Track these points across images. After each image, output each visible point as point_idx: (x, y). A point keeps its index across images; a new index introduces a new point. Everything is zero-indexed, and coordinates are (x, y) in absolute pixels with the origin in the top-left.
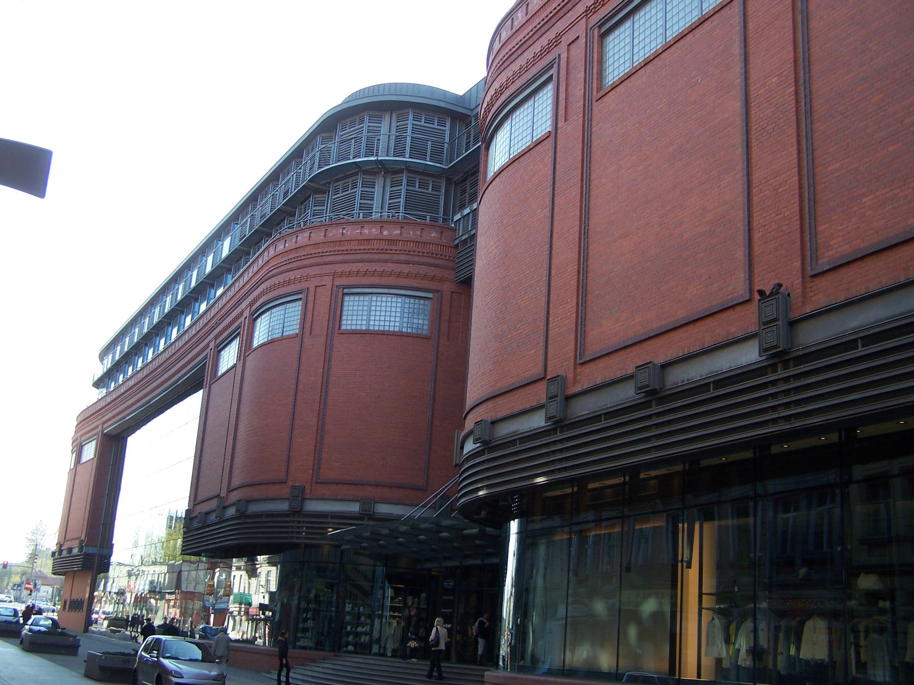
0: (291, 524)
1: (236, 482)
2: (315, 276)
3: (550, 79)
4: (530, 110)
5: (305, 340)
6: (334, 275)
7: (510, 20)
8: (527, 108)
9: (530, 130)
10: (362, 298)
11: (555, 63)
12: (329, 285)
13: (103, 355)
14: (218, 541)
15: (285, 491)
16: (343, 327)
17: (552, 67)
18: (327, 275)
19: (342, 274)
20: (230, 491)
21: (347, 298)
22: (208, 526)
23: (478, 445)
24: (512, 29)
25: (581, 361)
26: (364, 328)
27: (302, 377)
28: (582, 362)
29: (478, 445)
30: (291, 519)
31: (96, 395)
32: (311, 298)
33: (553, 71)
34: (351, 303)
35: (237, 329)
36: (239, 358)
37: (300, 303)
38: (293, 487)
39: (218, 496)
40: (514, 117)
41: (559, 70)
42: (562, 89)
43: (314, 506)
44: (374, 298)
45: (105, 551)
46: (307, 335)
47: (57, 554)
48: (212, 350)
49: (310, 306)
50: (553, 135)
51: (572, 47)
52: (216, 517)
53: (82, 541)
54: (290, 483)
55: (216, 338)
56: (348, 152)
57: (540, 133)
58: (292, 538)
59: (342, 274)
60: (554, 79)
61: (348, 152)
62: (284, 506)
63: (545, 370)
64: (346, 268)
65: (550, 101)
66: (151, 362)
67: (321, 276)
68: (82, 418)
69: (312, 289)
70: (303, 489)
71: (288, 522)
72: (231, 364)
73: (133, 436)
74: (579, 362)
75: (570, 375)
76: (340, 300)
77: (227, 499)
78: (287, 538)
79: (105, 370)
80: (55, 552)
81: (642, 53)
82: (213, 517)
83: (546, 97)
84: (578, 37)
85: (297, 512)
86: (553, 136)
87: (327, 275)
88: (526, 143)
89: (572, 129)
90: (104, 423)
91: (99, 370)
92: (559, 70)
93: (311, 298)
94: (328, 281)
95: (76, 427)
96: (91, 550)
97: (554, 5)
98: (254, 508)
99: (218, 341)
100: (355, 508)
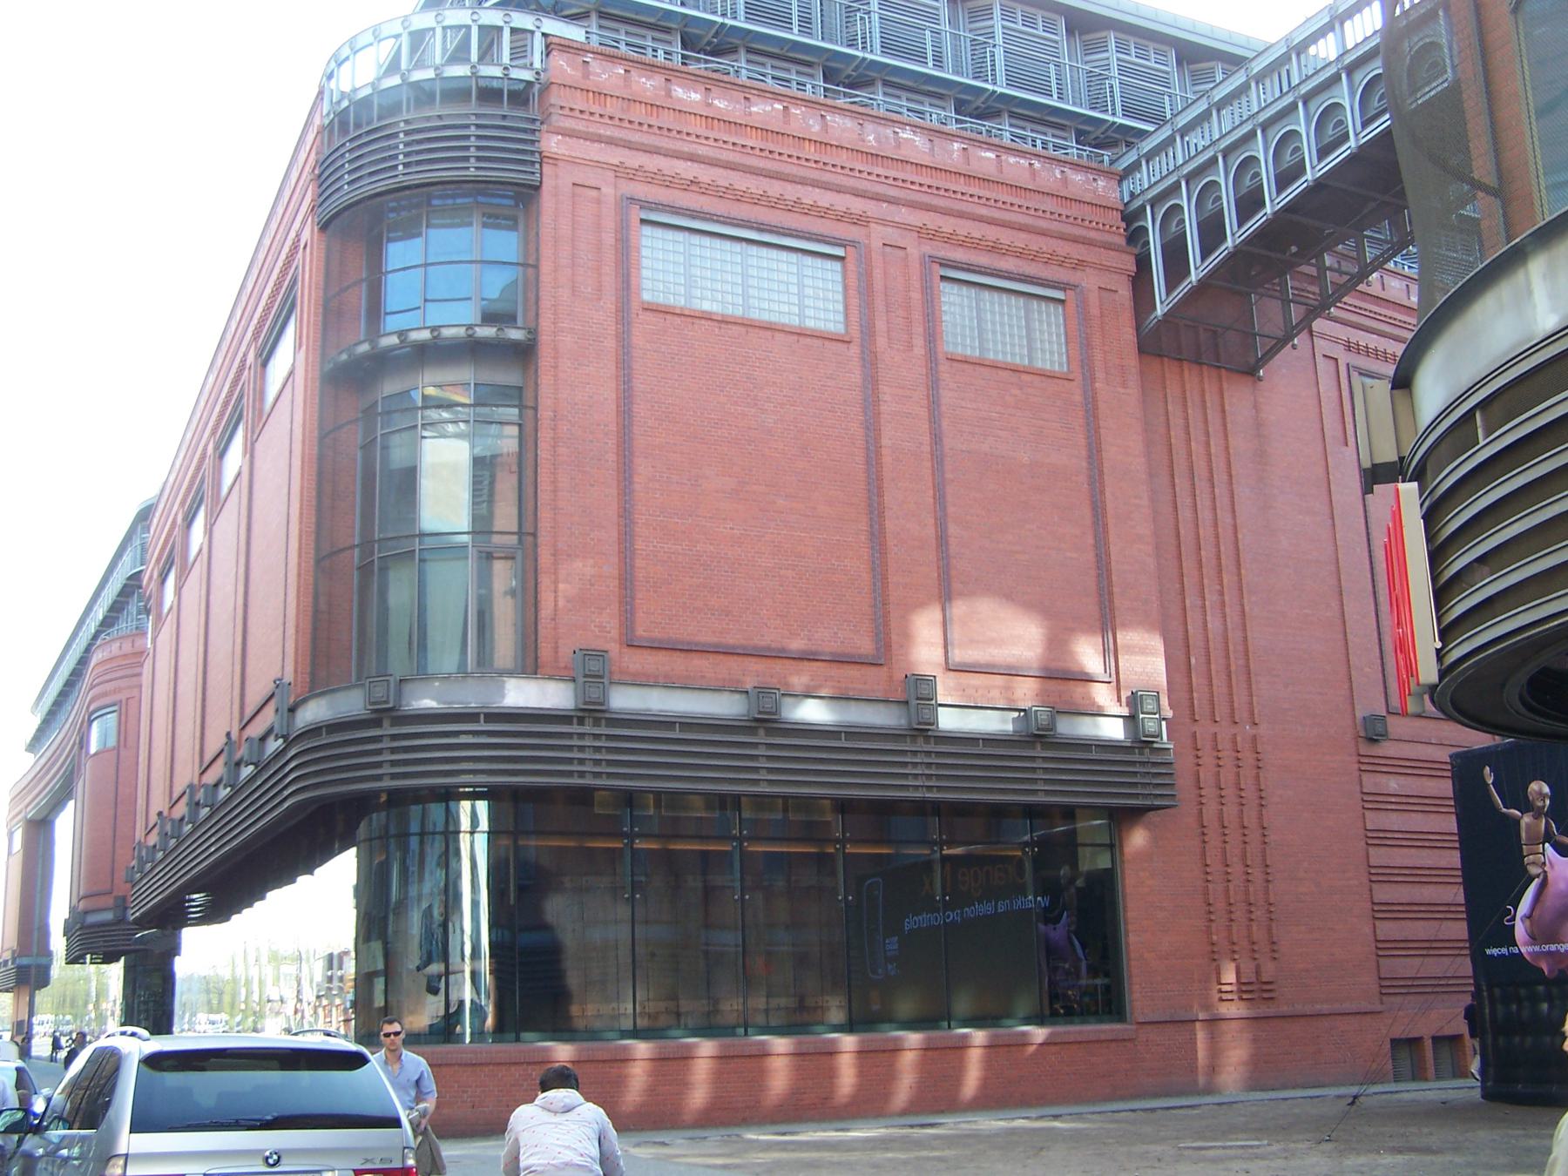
0: (575, 742)
27: (120, 788)
30: (575, 729)
37: (115, 714)
38: (116, 898)
45: (43, 961)
46: (122, 749)
47: (10, 963)
49: (123, 718)
53: (14, 952)
54: (115, 894)
56: (325, 186)
58: (582, 774)
61: (325, 186)
62: (108, 916)
68: (12, 796)
69: (124, 702)
70: (124, 899)
71: (570, 735)
78: (570, 774)
80: (7, 961)
85: (591, 712)
96: (25, 961)
98: (91, 919)
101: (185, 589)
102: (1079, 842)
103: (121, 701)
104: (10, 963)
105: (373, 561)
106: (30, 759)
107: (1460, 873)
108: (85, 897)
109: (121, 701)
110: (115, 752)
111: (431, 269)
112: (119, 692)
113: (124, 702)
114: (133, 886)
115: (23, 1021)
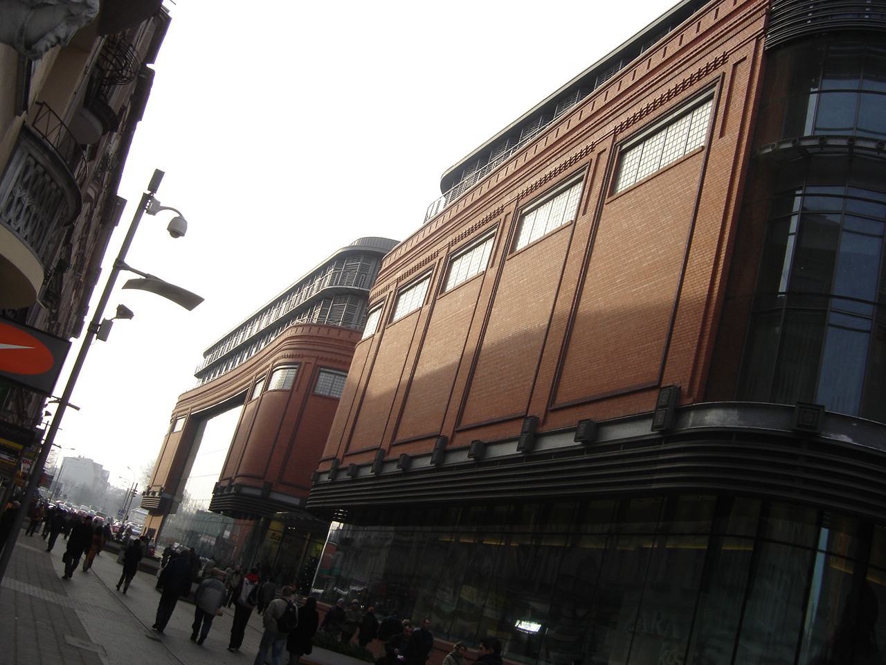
1: (240, 472)
2: (307, 356)
3: (264, 379)
4: (688, 124)
5: (293, 395)
6: (318, 357)
7: (715, 9)
8: (685, 121)
9: (683, 144)
10: (330, 375)
11: (718, 81)
12: (313, 363)
13: (206, 354)
14: (543, 478)
15: (261, 484)
16: (316, 391)
17: (714, 85)
18: (313, 357)
19: (322, 359)
20: (393, 445)
21: (322, 373)
22: (320, 485)
23: (579, 443)
24: (698, 31)
25: (552, 408)
26: (327, 394)
28: (457, 431)
29: (579, 443)
31: (195, 383)
32: (302, 369)
33: (716, 89)
34: (323, 376)
35: (493, 229)
36: (491, 263)
37: (295, 370)
39: (334, 458)
40: (646, 144)
41: (588, 172)
42: (431, 282)
43: (276, 496)
44: (337, 377)
47: (157, 494)
48: (392, 294)
49: (300, 374)
50: (705, 151)
51: (602, 156)
52: (372, 472)
53: (162, 489)
55: (450, 245)
57: (692, 147)
59: (322, 359)
60: (715, 96)
62: (258, 493)
63: (661, 380)
64: (325, 355)
65: (708, 118)
66: (264, 349)
67: (309, 356)
68: (181, 399)
69: (303, 364)
72: (414, 308)
73: (211, 420)
74: (549, 409)
75: (541, 418)
76: (317, 374)
77: (452, 441)
79: (204, 368)
81: (667, 160)
82: (368, 472)
83: (705, 112)
84: (746, 57)
86: (573, 223)
87: (313, 357)
88: (678, 154)
89: (586, 221)
90: (192, 408)
91: (202, 363)
92: (588, 172)
93: (302, 369)
94: (313, 361)
95: (450, 181)
97: (755, 4)
98: (246, 491)
99: (453, 249)
100: (296, 502)
101: (131, 266)
102: (69, 402)
103: (301, 363)
104: (157, 494)
105: (782, 309)
106: (195, 383)
107: (868, 310)
108: (242, 476)
109: (301, 363)
110: (289, 393)
111: (823, 94)
112: (302, 357)
113: (303, 364)
114: (315, 486)
115: (154, 530)
